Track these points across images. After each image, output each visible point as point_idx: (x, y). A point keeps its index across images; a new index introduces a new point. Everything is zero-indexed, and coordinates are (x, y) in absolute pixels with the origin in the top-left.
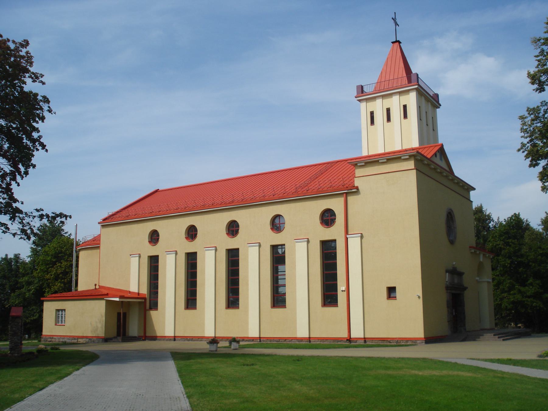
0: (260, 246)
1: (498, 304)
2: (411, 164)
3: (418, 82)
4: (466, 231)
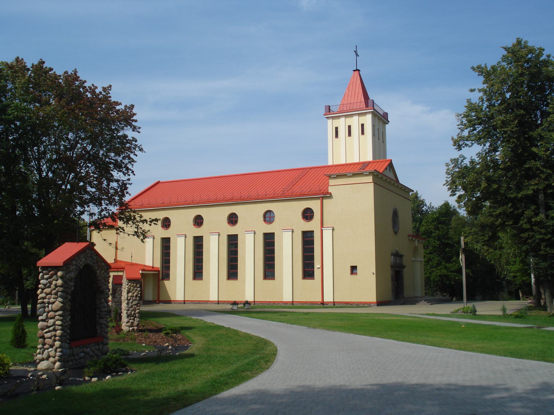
0: (255, 233)
1: (427, 277)
2: (370, 179)
3: (373, 107)
4: (407, 223)
